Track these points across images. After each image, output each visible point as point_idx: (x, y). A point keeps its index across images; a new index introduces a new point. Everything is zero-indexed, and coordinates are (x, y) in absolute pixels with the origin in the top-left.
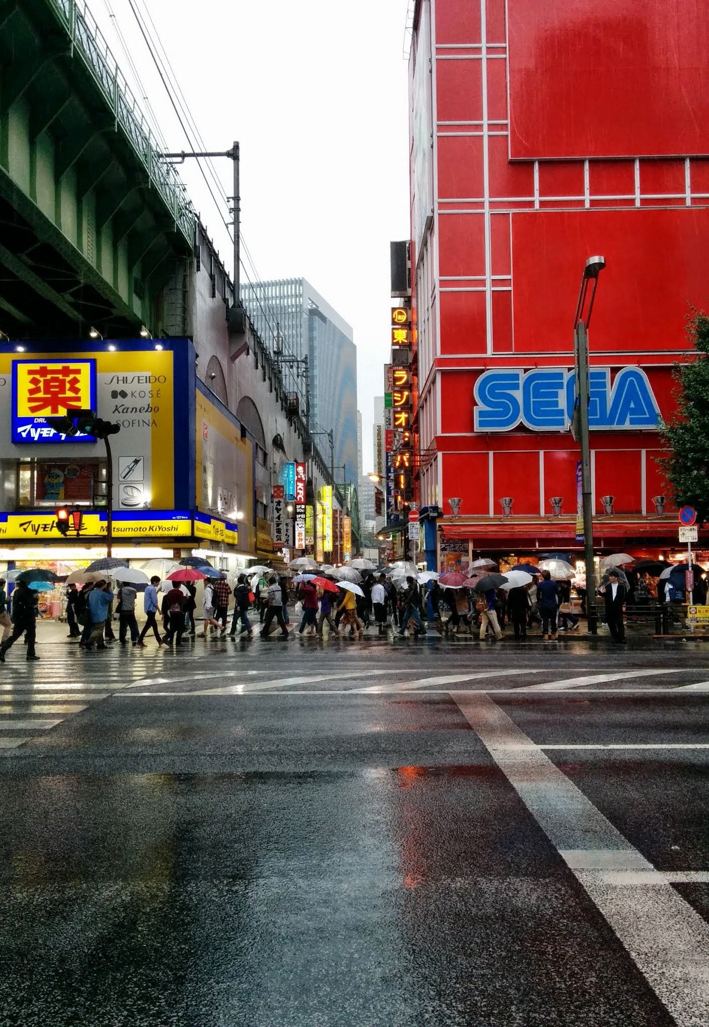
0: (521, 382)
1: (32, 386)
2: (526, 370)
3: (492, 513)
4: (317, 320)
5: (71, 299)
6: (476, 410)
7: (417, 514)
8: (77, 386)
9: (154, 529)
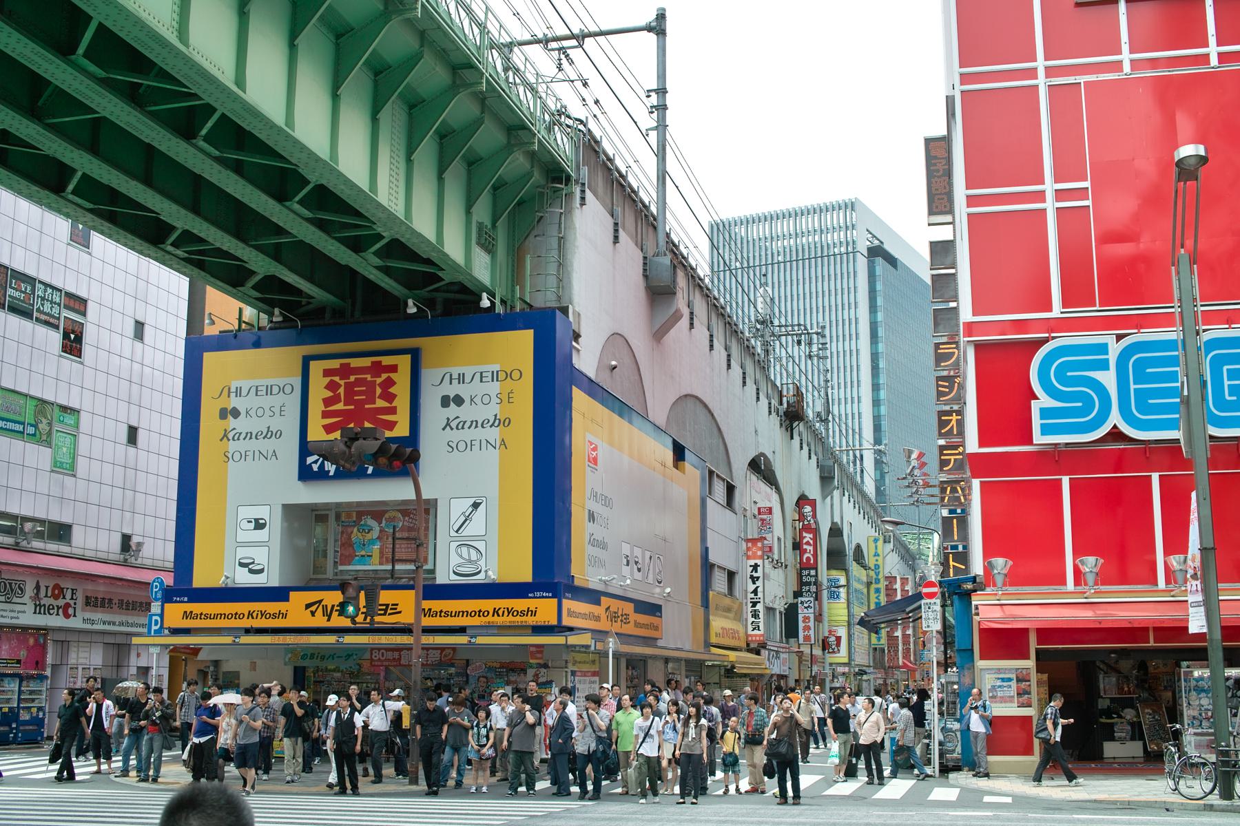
0: (1112, 357)
1: (329, 394)
2: (1119, 338)
3: (1161, 583)
4: (880, 264)
5: (377, 262)
6: (1035, 406)
7: (935, 586)
8: (392, 390)
9: (500, 612)
